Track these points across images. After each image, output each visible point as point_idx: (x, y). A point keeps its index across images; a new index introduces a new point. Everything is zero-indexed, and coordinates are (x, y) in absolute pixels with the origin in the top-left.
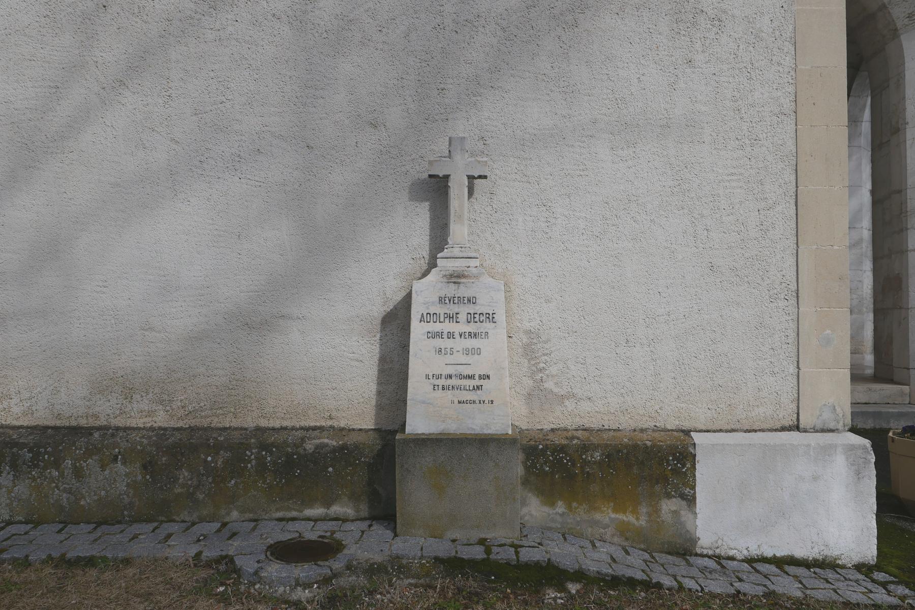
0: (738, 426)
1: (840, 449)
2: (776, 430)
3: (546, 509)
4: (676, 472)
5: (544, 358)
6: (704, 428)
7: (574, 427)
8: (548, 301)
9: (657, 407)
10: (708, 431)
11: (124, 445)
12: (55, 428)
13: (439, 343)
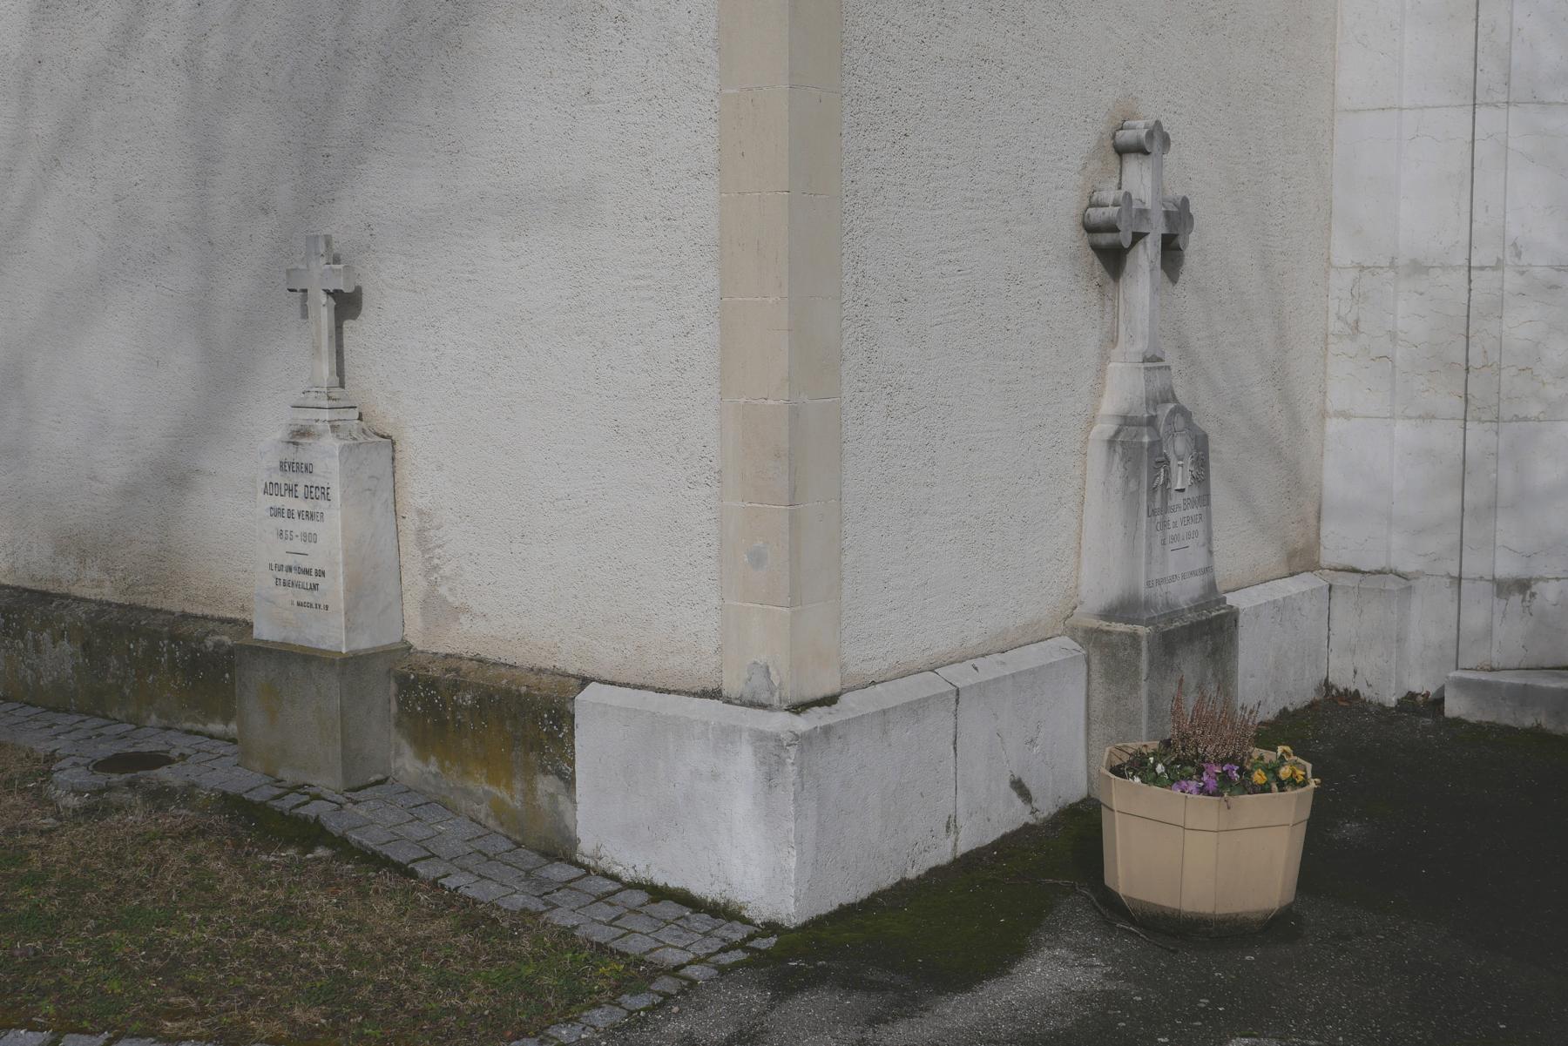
0: (648, 682)
1: (745, 735)
2: (695, 695)
3: (419, 764)
4: (551, 736)
5: (438, 551)
6: (609, 678)
7: (470, 655)
8: (440, 468)
9: (557, 639)
10: (613, 683)
11: (69, 619)
12: (31, 592)
13: (283, 523)
